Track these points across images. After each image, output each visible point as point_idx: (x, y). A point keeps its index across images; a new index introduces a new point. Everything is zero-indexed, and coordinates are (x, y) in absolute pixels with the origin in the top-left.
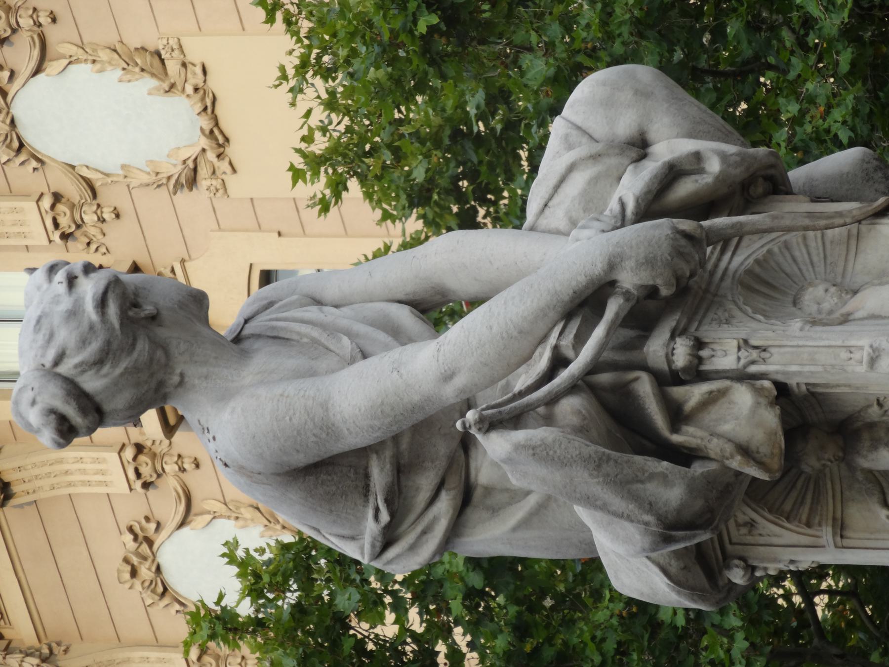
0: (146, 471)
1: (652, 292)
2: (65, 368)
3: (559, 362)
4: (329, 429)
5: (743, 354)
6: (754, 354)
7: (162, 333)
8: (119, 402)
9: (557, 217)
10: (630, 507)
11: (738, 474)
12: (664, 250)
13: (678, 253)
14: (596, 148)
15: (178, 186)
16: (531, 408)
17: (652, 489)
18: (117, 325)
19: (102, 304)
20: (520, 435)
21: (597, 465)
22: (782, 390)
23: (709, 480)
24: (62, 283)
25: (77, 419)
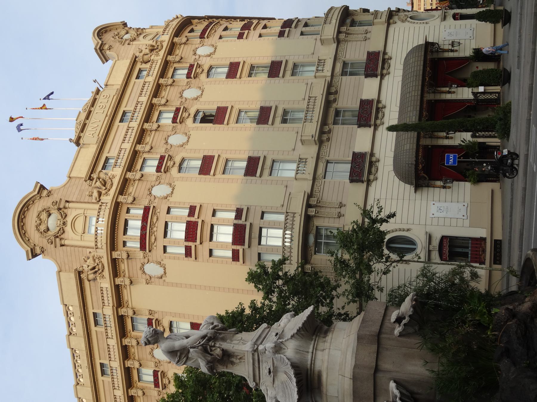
1: (211, 337)
2: (147, 337)
3: (200, 343)
4: (174, 347)
8: (152, 342)
9: (202, 329)
11: (217, 358)
13: (214, 333)
15: (160, 278)
16: (196, 347)
17: (207, 358)
19: (153, 331)
20: (194, 349)
21: (202, 354)
25: (147, 343)
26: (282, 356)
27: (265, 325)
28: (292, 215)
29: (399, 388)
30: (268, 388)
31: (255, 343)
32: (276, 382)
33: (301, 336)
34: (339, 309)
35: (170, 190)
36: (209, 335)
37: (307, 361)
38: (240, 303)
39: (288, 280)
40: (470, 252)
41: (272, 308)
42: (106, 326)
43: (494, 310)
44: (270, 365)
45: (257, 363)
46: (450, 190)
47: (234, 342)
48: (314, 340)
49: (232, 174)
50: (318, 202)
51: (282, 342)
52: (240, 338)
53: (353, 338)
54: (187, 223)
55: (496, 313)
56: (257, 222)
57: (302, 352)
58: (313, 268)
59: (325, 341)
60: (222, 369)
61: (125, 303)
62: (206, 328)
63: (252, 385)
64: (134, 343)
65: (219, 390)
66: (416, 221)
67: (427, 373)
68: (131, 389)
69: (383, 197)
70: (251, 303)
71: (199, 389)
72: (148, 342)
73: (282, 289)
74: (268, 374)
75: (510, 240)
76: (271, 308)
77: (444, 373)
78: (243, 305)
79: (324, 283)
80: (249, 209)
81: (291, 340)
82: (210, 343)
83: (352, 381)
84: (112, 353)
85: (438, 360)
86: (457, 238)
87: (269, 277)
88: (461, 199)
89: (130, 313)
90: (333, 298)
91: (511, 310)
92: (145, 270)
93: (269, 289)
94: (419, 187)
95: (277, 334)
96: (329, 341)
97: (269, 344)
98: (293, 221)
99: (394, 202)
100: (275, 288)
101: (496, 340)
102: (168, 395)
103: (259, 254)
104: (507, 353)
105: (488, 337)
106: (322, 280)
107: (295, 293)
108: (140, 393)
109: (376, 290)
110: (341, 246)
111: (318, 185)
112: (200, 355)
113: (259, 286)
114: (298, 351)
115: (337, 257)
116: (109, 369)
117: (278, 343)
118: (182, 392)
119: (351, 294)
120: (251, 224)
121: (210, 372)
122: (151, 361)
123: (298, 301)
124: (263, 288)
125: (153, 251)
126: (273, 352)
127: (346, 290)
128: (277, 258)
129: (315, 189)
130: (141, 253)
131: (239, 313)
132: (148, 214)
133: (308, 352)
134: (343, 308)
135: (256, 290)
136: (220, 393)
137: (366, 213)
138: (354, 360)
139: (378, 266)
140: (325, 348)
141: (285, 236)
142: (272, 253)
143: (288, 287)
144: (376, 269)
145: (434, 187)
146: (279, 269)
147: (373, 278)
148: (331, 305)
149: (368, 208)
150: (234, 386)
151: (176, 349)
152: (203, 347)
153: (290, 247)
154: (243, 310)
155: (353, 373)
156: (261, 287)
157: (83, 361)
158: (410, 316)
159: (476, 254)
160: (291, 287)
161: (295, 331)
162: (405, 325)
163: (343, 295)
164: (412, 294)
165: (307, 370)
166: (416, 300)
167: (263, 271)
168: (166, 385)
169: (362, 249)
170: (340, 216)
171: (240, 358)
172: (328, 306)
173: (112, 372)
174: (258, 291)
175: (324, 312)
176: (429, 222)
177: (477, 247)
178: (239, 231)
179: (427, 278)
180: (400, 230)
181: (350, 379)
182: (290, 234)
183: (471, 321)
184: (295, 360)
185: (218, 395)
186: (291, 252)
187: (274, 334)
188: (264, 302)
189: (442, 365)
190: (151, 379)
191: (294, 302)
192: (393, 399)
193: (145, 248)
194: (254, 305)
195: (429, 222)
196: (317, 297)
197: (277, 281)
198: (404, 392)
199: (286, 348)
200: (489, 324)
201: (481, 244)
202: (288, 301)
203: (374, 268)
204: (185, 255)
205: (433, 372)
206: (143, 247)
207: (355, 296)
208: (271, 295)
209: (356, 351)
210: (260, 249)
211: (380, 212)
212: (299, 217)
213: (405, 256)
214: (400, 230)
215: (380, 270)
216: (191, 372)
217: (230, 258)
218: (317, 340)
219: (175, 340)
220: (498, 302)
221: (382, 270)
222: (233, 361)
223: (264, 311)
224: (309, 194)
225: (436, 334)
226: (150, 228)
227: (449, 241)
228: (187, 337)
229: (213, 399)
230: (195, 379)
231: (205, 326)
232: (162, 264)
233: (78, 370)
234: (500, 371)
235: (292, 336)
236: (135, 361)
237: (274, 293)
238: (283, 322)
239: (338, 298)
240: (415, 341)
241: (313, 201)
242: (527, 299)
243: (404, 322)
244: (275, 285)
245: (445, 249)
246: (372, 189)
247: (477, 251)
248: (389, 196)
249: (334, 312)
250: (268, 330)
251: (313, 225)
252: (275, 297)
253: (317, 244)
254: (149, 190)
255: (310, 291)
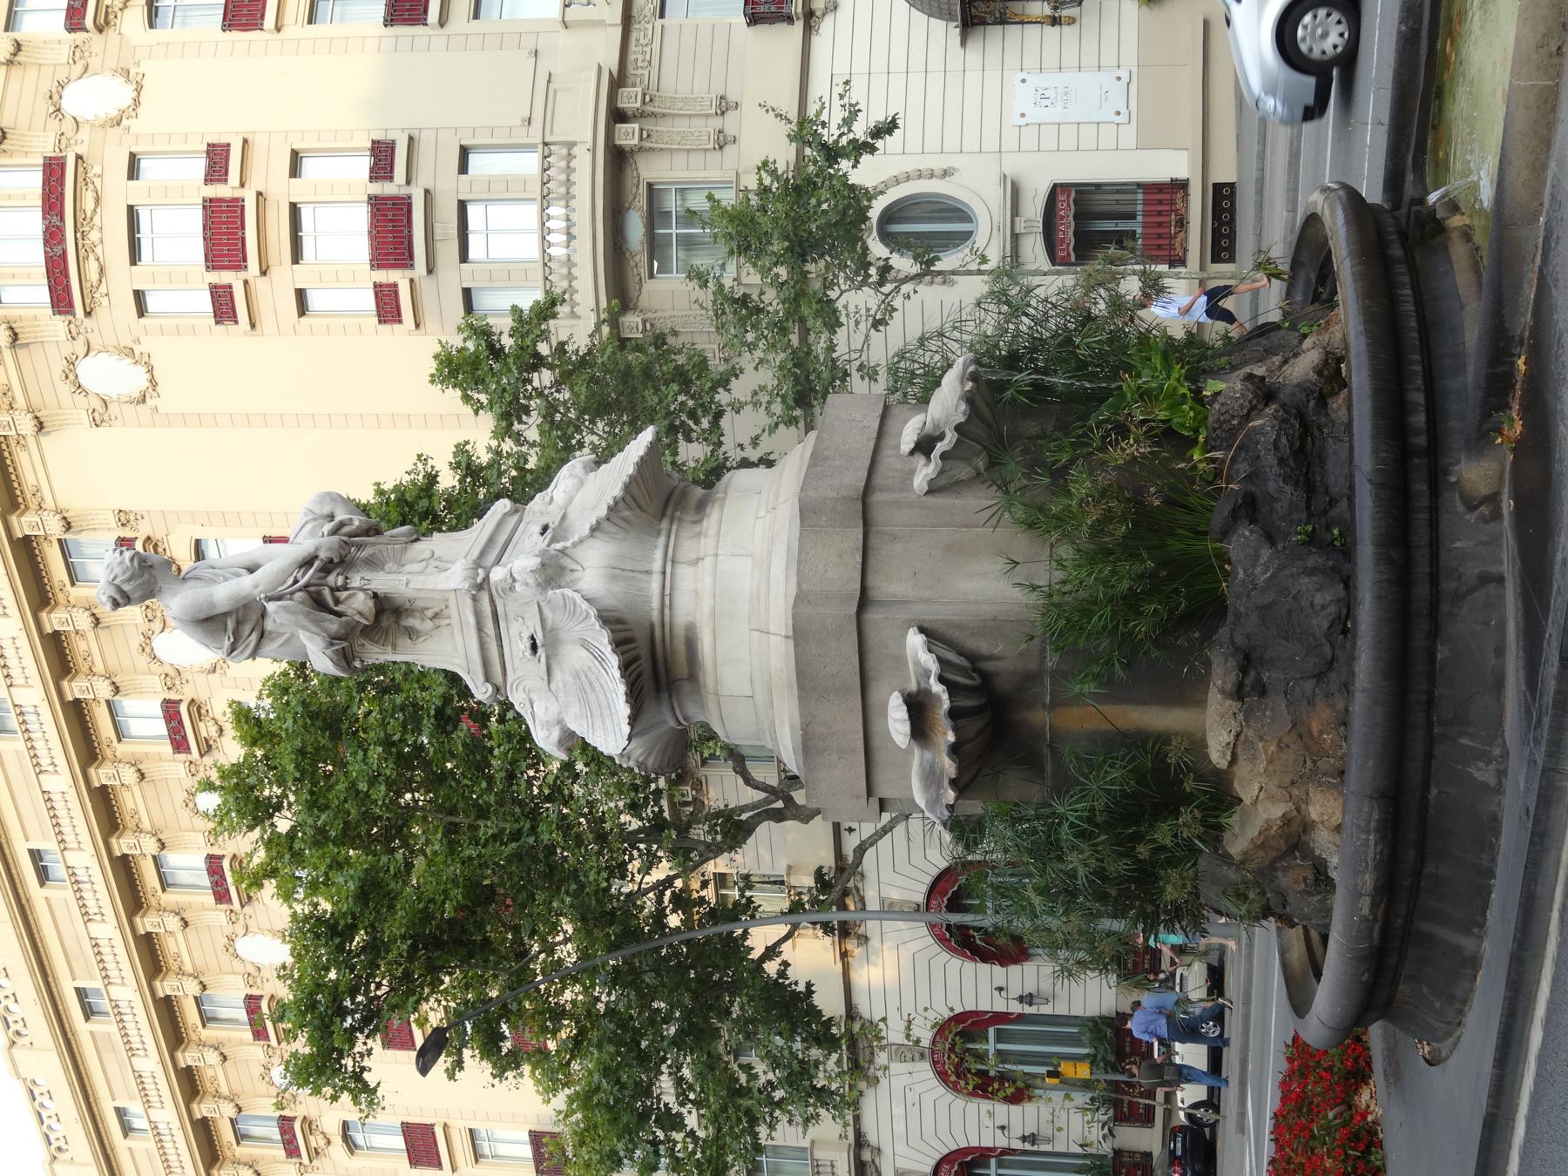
0: (233, 919)
1: (331, 561)
3: (296, 581)
4: (212, 605)
7: (154, 572)
10: (319, 631)
12: (336, 546)
15: (138, 402)
19: (132, 559)
20: (280, 603)
21: (307, 614)
22: (375, 595)
23: (347, 623)
26: (568, 592)
27: (503, 505)
28: (564, 151)
29: (934, 648)
30: (534, 696)
31: (478, 564)
32: (557, 675)
33: (622, 524)
34: (741, 446)
35: (128, 92)
36: (323, 555)
37: (648, 601)
38: (419, 456)
39: (571, 368)
40: (1139, 230)
41: (526, 461)
42: (77, 882)
43: (1211, 387)
44: (533, 626)
45: (490, 623)
46: (1074, 28)
47: (408, 568)
48: (664, 534)
49: (342, 20)
50: (647, 99)
51: (563, 551)
52: (427, 555)
53: (787, 511)
54: (204, 207)
55: (1217, 394)
56: (449, 187)
57: (631, 574)
58: (648, 325)
59: (699, 534)
60: (377, 654)
61: (29, 496)
62: (312, 534)
63: (481, 692)
64: (83, 621)
65: (382, 734)
66: (971, 143)
67: (1017, 594)
68: (97, 768)
69: (860, 66)
70: (455, 455)
71: (320, 738)
72: (123, 597)
73: (555, 399)
74: (528, 652)
75: (1261, 181)
76: (522, 461)
77: (1066, 589)
78: (430, 462)
79: (686, 368)
80: (416, 141)
81: (591, 542)
82: (331, 579)
83: (791, 643)
84: (64, 821)
85: (1048, 553)
86: (1098, 186)
87: (506, 364)
88: (1109, 57)
89: (54, 527)
90: (719, 415)
91: (1262, 379)
92: (82, 380)
93: (510, 403)
94: (973, 24)
95: (545, 529)
96: (712, 531)
97: (522, 561)
98: (569, 170)
99: (897, 82)
100: (530, 398)
101: (1217, 474)
102: (220, 769)
103: (467, 293)
104: (1250, 508)
105: (1194, 467)
106: (681, 360)
107: (598, 408)
108: (129, 775)
109: (855, 376)
110: (731, 252)
111: (642, 41)
112: (302, 619)
113: (476, 396)
114: (616, 572)
115: (721, 286)
116: (13, 715)
117: (552, 556)
118: (266, 757)
119: (779, 399)
120: (427, 192)
121: (343, 670)
122: (150, 673)
123: (609, 432)
124: (491, 404)
125: (100, 313)
126: (539, 585)
127: (762, 388)
128: (527, 299)
129: (632, 57)
130: (59, 324)
131: (422, 489)
132: (62, 184)
133: (648, 572)
134: (755, 442)
135: (468, 410)
136: (387, 743)
137: (804, 130)
138: (794, 579)
139: (856, 301)
140: (701, 555)
141: (547, 224)
142: (509, 284)
143: (571, 389)
144: (852, 309)
145: (1022, 23)
146: (538, 336)
147: (846, 341)
148: (714, 435)
149: (811, 111)
150: (428, 715)
151: (221, 609)
152: (309, 593)
153: (569, 262)
154: (432, 479)
155: (795, 618)
156: (483, 398)
157: (64, 1102)
158: (958, 428)
159: (1160, 236)
160: (584, 389)
161: (603, 511)
162: (944, 456)
163: (755, 404)
164: (960, 361)
165: (652, 627)
166: (974, 377)
167: (484, 344)
168: (211, 742)
169: (801, 249)
170: (722, 142)
171: (436, 616)
172: (706, 439)
173: (24, 722)
174: (476, 412)
175: (697, 461)
176: (1010, 143)
177: (1160, 213)
178: (391, 221)
179: (1008, 303)
180: (920, 175)
181: (787, 637)
182: (564, 217)
183: (1143, 422)
184: (610, 602)
185: (380, 749)
186: (570, 277)
187: (538, 529)
188: (499, 445)
189: (1061, 564)
190: (161, 728)
191: (595, 439)
192: (919, 683)
193: (71, 304)
194: (465, 459)
195: (1010, 143)
196: (669, 413)
197: (536, 374)
198: (952, 657)
199: (579, 568)
200: (1196, 432)
201: (1172, 202)
202: (578, 437)
203: (846, 307)
204: (215, 316)
205: (1034, 590)
206: (61, 301)
207: (791, 403)
208: (520, 422)
209: (799, 554)
210: (467, 276)
211: (848, 122)
212: (589, 156)
213: (939, 259)
214: (920, 175)
215: (863, 312)
216: (285, 691)
217: (368, 316)
218: (674, 531)
219: (212, 581)
220: (1223, 360)
221: (868, 310)
222: (412, 628)
223: (500, 475)
224: (615, 74)
225: (1037, 474)
226: (76, 232)
227: (1075, 201)
228: (251, 570)
229: (366, 764)
230: (300, 709)
231: (309, 527)
232: (137, 353)
233: (42, 1105)
234: (1230, 564)
235: (595, 529)
236: (95, 678)
237: (528, 413)
238: (561, 487)
239: (738, 412)
240: (978, 501)
241: (630, 99)
242: (1307, 343)
243: (940, 447)
244: (529, 388)
245: (1062, 228)
246: (820, 43)
247: (1160, 225)
248: (879, 65)
249: (726, 459)
250: (516, 518)
251: (635, 181)
252: (534, 427)
253: (655, 246)
254: (51, 97)
255: (644, 397)
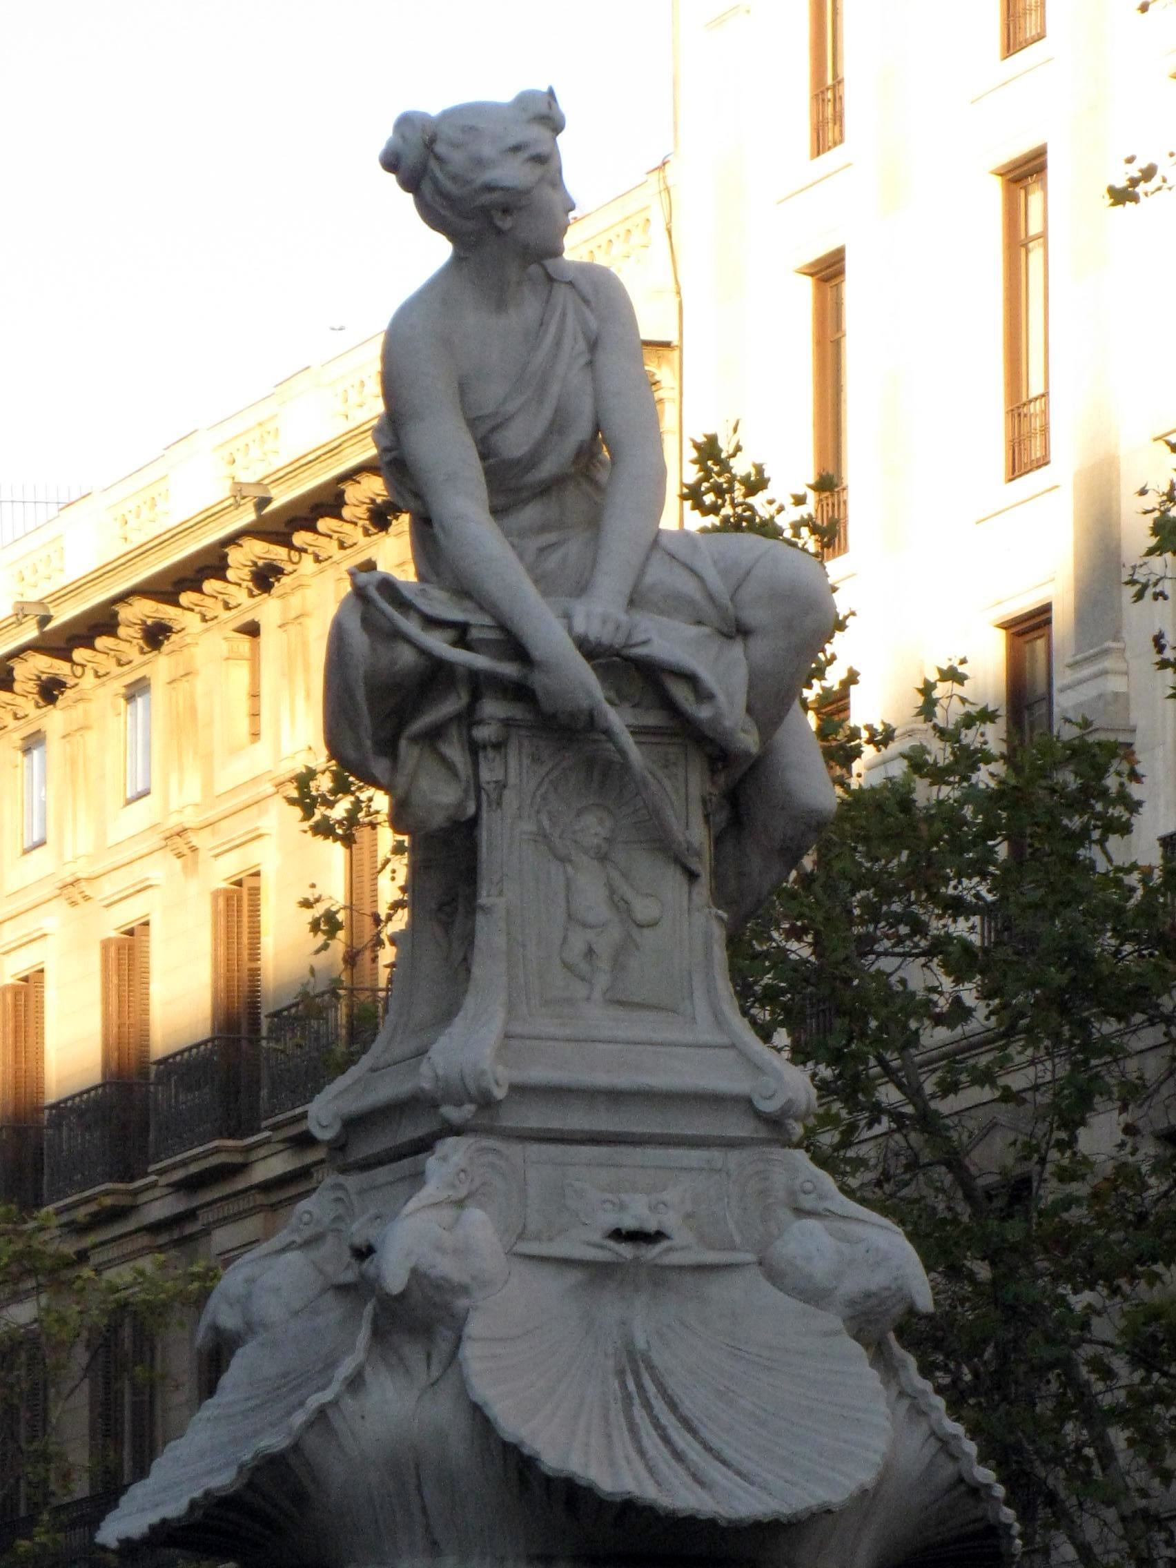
5: (493, 785)
6: (494, 796)
14: (725, 599)
18: (477, 203)
22: (474, 822)
24: (673, 388)
